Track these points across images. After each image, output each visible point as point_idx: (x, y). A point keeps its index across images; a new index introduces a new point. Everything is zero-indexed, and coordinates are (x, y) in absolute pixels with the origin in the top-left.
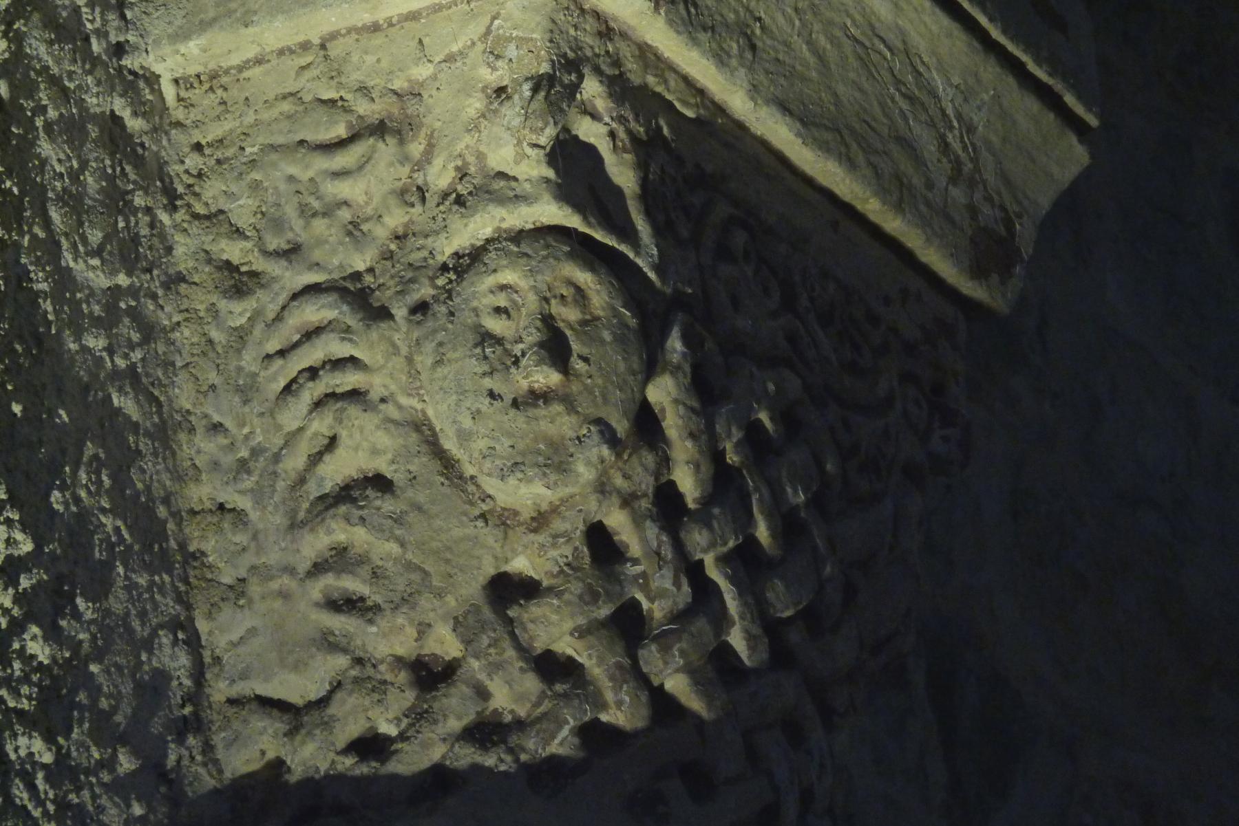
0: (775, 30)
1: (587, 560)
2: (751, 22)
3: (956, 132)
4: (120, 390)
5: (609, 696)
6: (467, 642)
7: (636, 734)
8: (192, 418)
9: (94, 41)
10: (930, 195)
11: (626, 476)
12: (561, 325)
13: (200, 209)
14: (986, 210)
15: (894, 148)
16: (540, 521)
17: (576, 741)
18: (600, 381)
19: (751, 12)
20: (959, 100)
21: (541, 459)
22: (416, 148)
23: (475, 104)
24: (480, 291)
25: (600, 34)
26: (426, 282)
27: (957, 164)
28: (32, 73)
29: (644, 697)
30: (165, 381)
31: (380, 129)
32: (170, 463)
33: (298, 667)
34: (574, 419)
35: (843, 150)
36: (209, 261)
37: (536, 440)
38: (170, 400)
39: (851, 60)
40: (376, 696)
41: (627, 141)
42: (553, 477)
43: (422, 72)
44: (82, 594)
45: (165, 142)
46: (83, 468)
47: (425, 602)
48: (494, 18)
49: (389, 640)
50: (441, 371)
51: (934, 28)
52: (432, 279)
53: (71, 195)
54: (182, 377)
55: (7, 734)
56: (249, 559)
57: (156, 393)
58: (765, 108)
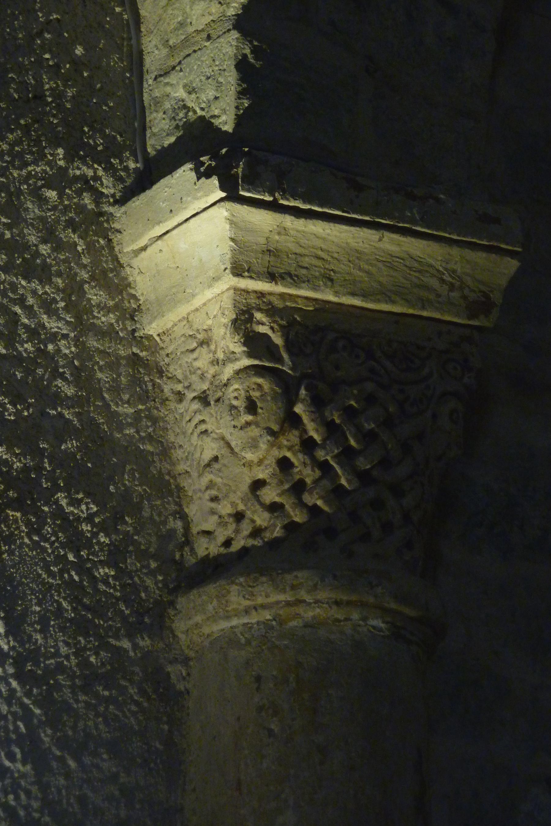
1: (278, 471)
2: (328, 272)
3: (447, 275)
5: (292, 514)
6: (246, 505)
7: (304, 523)
8: (175, 444)
9: (120, 333)
10: (440, 299)
11: (288, 441)
12: (254, 398)
13: (170, 375)
16: (260, 462)
17: (283, 531)
18: (267, 415)
19: (327, 269)
20: (444, 265)
22: (213, 347)
24: (230, 392)
25: (258, 298)
26: (219, 391)
28: (91, 353)
29: (305, 511)
30: (163, 435)
32: (169, 461)
33: (206, 521)
34: (259, 429)
37: (248, 439)
38: (167, 440)
39: (383, 268)
40: (224, 528)
42: (253, 450)
43: (210, 322)
45: (158, 356)
46: (126, 474)
47: (231, 495)
49: (225, 509)
51: (421, 246)
52: (221, 389)
54: (170, 431)
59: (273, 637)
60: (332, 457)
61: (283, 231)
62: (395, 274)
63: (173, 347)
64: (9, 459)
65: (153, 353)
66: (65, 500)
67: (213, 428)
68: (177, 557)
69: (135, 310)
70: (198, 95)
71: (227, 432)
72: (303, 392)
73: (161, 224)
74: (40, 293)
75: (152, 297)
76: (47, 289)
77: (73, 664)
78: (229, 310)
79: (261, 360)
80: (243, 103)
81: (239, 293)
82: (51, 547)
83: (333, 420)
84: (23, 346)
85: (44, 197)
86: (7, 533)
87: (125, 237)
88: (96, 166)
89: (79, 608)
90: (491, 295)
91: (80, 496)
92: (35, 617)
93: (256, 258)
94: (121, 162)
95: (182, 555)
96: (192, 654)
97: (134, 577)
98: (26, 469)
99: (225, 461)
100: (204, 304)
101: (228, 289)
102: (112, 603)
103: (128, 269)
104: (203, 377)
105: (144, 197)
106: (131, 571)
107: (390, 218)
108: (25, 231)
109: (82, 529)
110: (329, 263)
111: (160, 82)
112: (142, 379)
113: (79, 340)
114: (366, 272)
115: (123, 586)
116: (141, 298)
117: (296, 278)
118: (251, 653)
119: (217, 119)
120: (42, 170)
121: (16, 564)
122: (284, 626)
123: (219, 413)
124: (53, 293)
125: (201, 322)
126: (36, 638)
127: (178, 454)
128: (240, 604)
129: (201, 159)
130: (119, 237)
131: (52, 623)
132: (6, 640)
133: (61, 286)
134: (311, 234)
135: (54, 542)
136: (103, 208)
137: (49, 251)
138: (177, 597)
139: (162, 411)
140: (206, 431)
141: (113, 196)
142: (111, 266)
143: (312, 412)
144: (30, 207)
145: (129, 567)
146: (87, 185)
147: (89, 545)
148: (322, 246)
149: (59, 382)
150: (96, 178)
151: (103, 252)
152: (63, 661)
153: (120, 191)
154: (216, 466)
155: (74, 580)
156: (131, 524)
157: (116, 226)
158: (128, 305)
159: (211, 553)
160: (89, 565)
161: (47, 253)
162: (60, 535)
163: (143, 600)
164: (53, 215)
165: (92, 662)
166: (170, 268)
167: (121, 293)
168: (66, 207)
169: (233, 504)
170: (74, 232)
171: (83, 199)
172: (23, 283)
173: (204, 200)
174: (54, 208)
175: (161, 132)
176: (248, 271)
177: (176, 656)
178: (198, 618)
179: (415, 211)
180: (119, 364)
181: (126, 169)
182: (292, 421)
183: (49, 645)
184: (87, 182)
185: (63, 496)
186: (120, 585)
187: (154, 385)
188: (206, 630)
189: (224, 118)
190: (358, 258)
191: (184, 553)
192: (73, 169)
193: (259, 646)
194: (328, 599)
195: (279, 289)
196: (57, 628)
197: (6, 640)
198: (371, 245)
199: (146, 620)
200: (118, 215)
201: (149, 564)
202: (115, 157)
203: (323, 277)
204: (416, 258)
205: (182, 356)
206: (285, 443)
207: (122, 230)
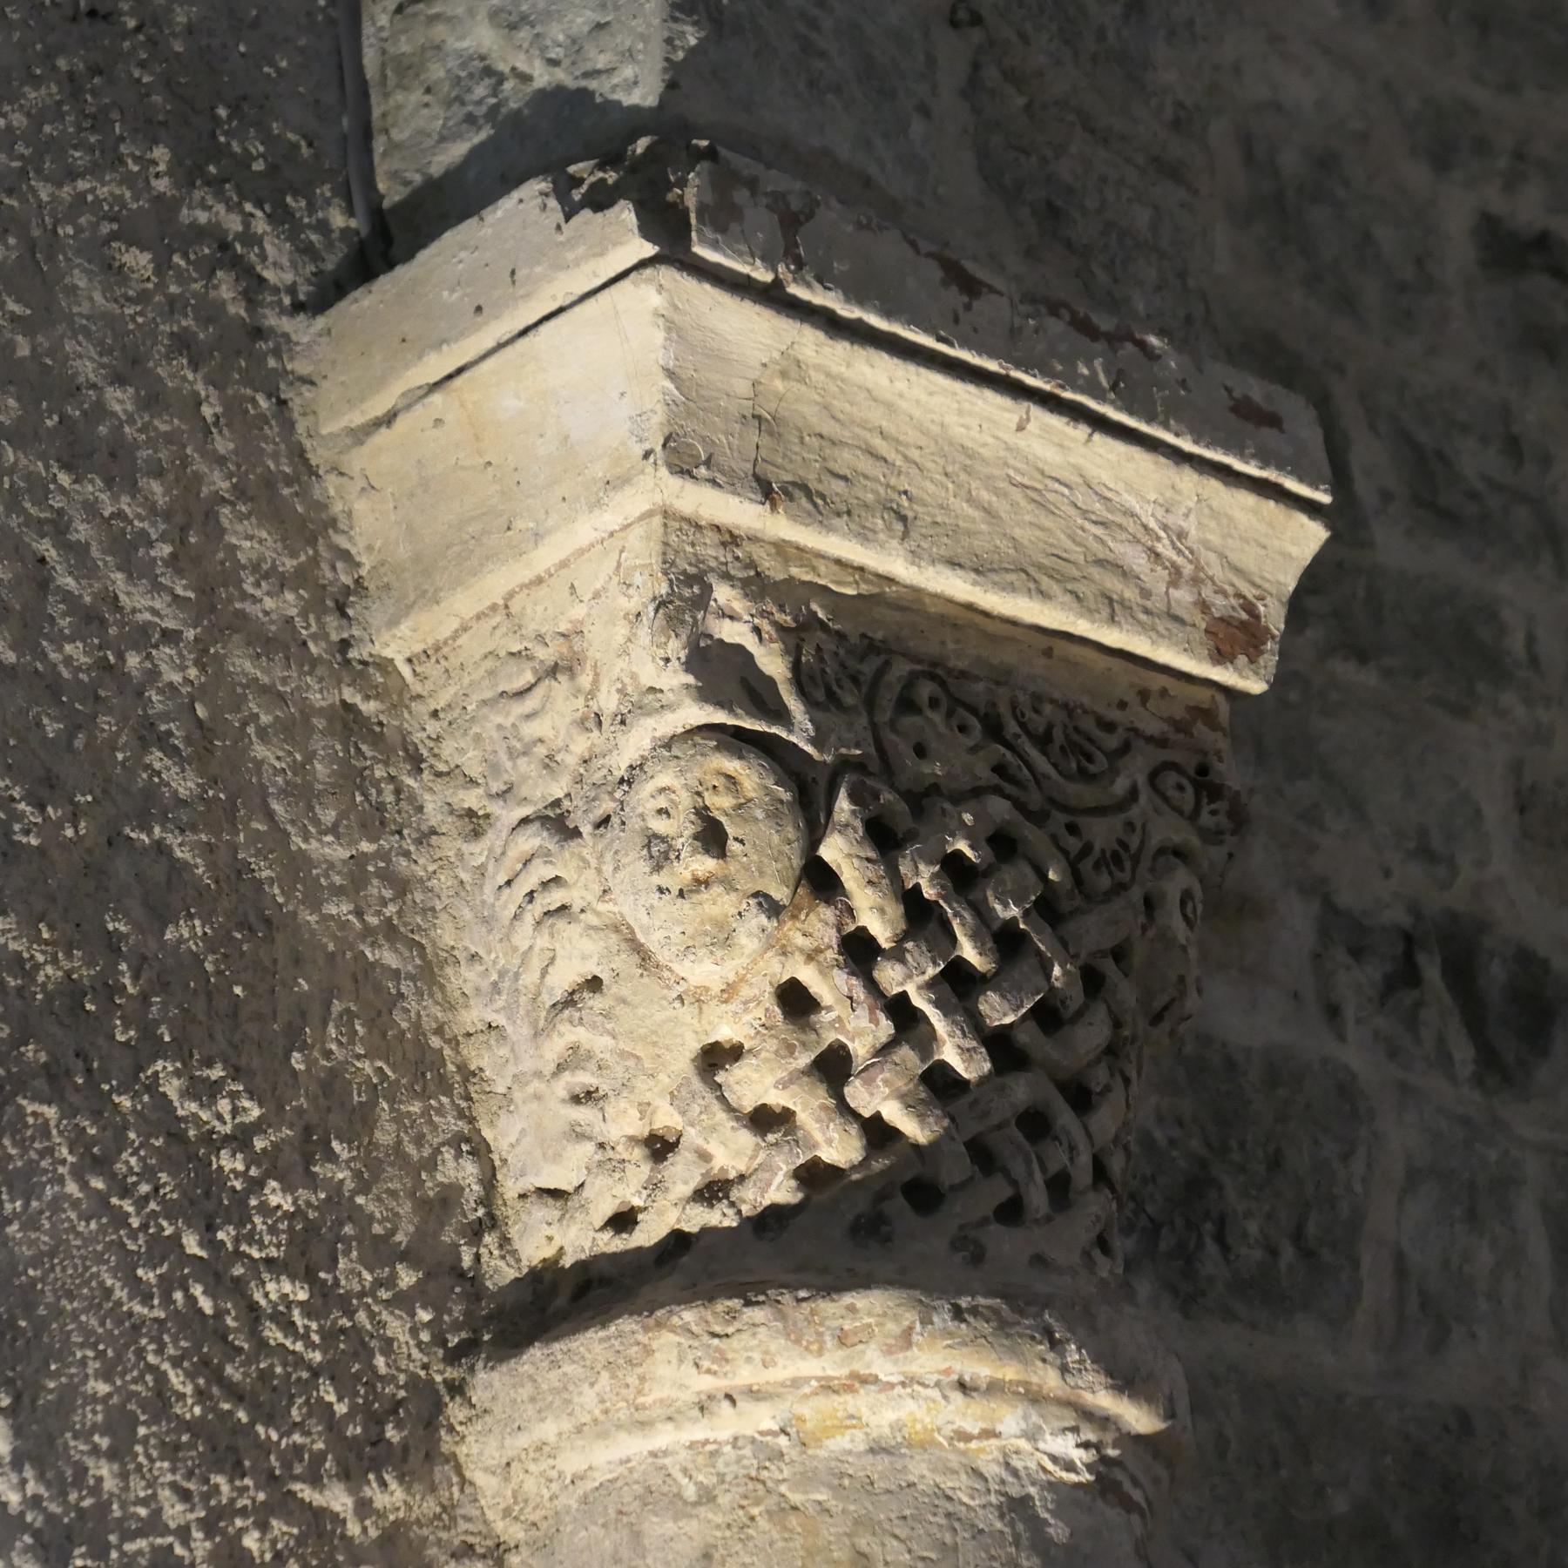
0: (925, 497)
1: (780, 1017)
2: (896, 496)
3: (1166, 542)
4: (373, 945)
5: (818, 1136)
6: (683, 1113)
8: (456, 953)
9: (311, 645)
10: (1149, 604)
13: (442, 768)
14: (1219, 601)
15: (1095, 572)
17: (793, 1183)
18: (755, 857)
19: (893, 488)
20: (1160, 513)
21: (708, 939)
22: (585, 680)
23: (622, 631)
24: (645, 797)
25: (724, 544)
26: (607, 797)
27: (1176, 571)
28: (239, 690)
29: (854, 1129)
31: (553, 671)
32: (439, 996)
33: (557, 1158)
34: (733, 896)
35: (1032, 586)
36: (451, 812)
37: (703, 923)
38: (434, 943)
39: (1023, 503)
40: (617, 1175)
41: (773, 632)
42: (719, 953)
43: (578, 611)
44: (336, 1138)
45: (406, 715)
46: (331, 1024)
47: (641, 1083)
48: (622, 551)
49: (623, 1123)
50: (620, 875)
51: (1112, 457)
52: (611, 794)
53: (296, 786)
54: (443, 916)
55: (253, 1284)
56: (511, 1069)
57: (417, 938)
58: (931, 568)
59: (784, 1480)
60: (920, 988)
61: (792, 368)
62: (1047, 521)
63: (452, 690)
64: (26, 955)
65: (394, 706)
66: (176, 1082)
67: (589, 897)
68: (467, 1260)
69: (347, 591)
70: (538, 29)
71: (626, 907)
72: (843, 805)
73: (445, 347)
74: (106, 514)
75: (403, 552)
76: (125, 503)
77: (199, 1554)
78: (647, 573)
79: (731, 711)
80: (683, 33)
81: (677, 525)
82: (138, 1213)
83: (917, 887)
84: (60, 649)
85: (117, 264)
86: (19, 1164)
87: (329, 391)
88: (248, 207)
89: (215, 1390)
90: (1262, 609)
91: (216, 1073)
92: (94, 1412)
93: (726, 434)
94: (311, 209)
95: (477, 1257)
96: (513, 1532)
97: (356, 1311)
98: (72, 991)
99: (625, 990)
100: (564, 564)
101: (649, 514)
102: (299, 1379)
103: (331, 483)
104: (553, 765)
105: (386, 285)
106: (349, 1295)
107: (1047, 373)
108: (69, 346)
109: (220, 1168)
110: (899, 473)
111: (415, 15)
112: (367, 772)
113: (205, 651)
114: (985, 509)
115: (331, 1336)
116: (364, 559)
117: (819, 502)
118: (718, 1527)
119: (604, 76)
120: (112, 194)
121: (42, 1254)
122: (810, 1452)
123: (608, 856)
124: (142, 519)
125: (546, 613)
126: (98, 1473)
127: (463, 978)
128: (683, 1387)
129: (572, 169)
130: (307, 395)
131: (142, 1431)
132: (14, 1478)
133: (161, 501)
134: (860, 387)
135: (146, 1199)
136: (265, 317)
137: (130, 407)
138: (472, 1370)
139: (421, 862)
140: (564, 908)
141: (292, 290)
142: (287, 470)
143: (868, 860)
144: (82, 284)
145: (343, 1282)
146: (227, 254)
147: (240, 1214)
148: (884, 424)
149: (156, 758)
150: (250, 239)
151: (267, 430)
152: (171, 1546)
153: (309, 282)
154: (596, 1002)
155: (200, 1311)
156: (348, 1161)
157: (301, 367)
158: (329, 575)
159: (569, 1250)
160: (238, 1271)
161: (125, 411)
162: (164, 1177)
163: (381, 1378)
164: (141, 314)
165: (250, 1551)
166: (463, 468)
167: (312, 541)
168: (172, 301)
169: (644, 1109)
170: (195, 365)
171: (216, 287)
172: (64, 479)
173: (588, 267)
174: (143, 298)
175: (420, 137)
176: (708, 463)
177: (470, 1539)
178: (548, 1430)
179: (1098, 363)
180: (310, 730)
181: (323, 227)
182: (821, 882)
183: (132, 1496)
184: (224, 246)
185: (170, 1069)
186: (320, 1331)
187: (398, 792)
188: (571, 1463)
189: (628, 72)
190: (965, 468)
191: (483, 1250)
192: (190, 208)
193: (742, 1507)
194: (940, 1372)
195: (781, 526)
196: (154, 1447)
197: (14, 1478)
198: (997, 438)
199: (391, 1433)
200: (305, 340)
201: (394, 1276)
202: (296, 193)
203: (885, 508)
204: (1098, 489)
205: (485, 710)
206: (799, 940)
207: (315, 378)
